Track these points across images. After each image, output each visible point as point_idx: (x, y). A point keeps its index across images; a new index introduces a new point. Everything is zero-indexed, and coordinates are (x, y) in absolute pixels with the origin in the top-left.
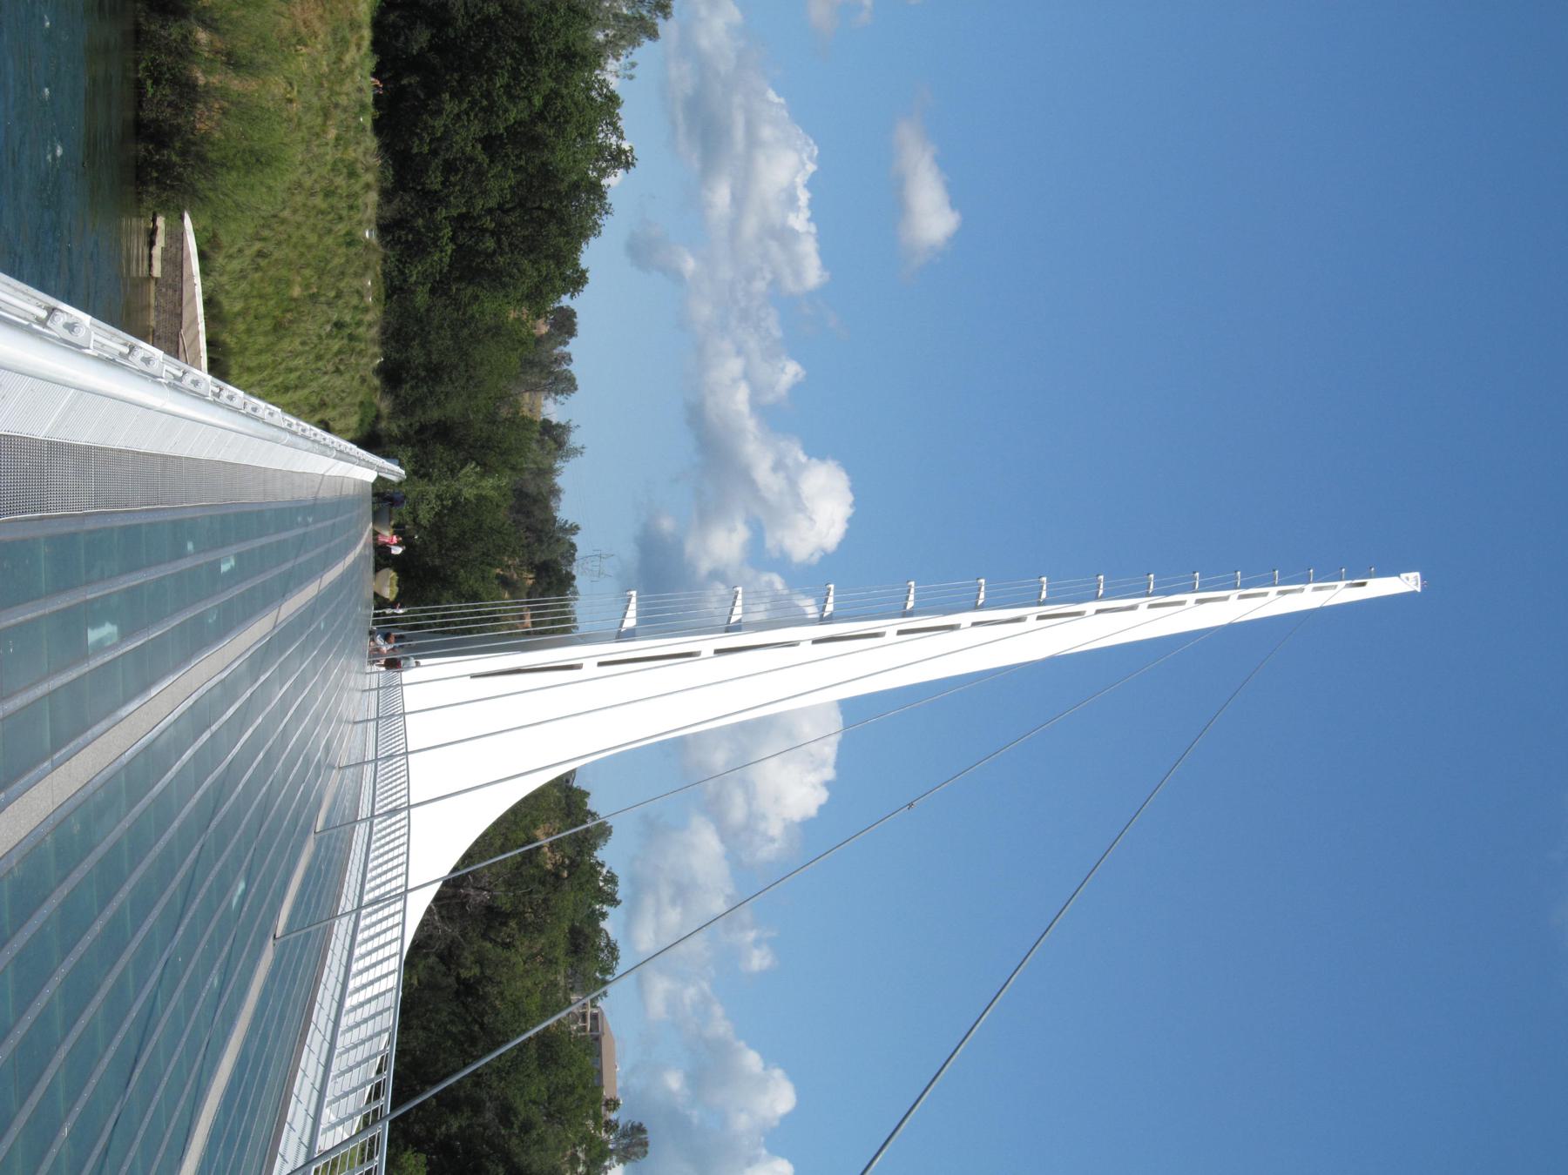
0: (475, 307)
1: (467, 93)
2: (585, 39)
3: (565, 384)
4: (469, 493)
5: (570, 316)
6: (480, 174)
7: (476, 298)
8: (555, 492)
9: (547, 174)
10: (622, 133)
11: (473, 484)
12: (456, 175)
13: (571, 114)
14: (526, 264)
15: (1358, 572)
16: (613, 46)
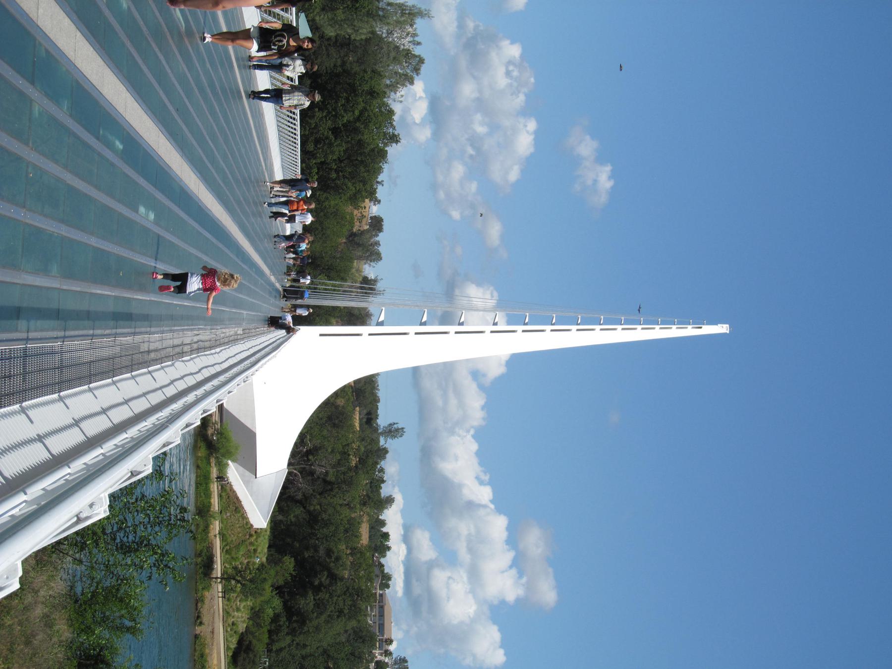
0: (327, 203)
3: (377, 257)
5: (380, 221)
6: (331, 145)
7: (327, 198)
9: (360, 143)
10: (395, 127)
12: (320, 144)
13: (372, 118)
14: (350, 184)
15: (699, 322)
16: (394, 87)
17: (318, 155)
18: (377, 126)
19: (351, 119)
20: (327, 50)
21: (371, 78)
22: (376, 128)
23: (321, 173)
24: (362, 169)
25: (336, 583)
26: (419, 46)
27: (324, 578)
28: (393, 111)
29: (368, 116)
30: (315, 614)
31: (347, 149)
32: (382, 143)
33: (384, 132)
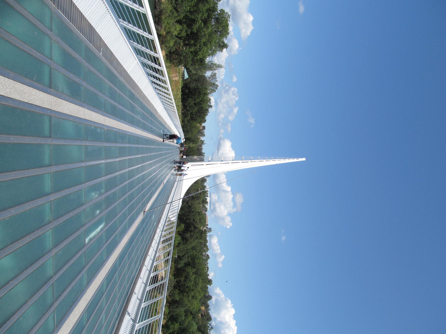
0: (193, 124)
1: (192, 98)
2: (207, 92)
3: (204, 135)
4: (191, 146)
6: (194, 108)
8: (202, 149)
9: (202, 108)
11: (192, 145)
15: (298, 157)
16: (210, 93)
20: (193, 82)
23: (191, 116)
27: (192, 228)
30: (190, 239)
32: (208, 107)
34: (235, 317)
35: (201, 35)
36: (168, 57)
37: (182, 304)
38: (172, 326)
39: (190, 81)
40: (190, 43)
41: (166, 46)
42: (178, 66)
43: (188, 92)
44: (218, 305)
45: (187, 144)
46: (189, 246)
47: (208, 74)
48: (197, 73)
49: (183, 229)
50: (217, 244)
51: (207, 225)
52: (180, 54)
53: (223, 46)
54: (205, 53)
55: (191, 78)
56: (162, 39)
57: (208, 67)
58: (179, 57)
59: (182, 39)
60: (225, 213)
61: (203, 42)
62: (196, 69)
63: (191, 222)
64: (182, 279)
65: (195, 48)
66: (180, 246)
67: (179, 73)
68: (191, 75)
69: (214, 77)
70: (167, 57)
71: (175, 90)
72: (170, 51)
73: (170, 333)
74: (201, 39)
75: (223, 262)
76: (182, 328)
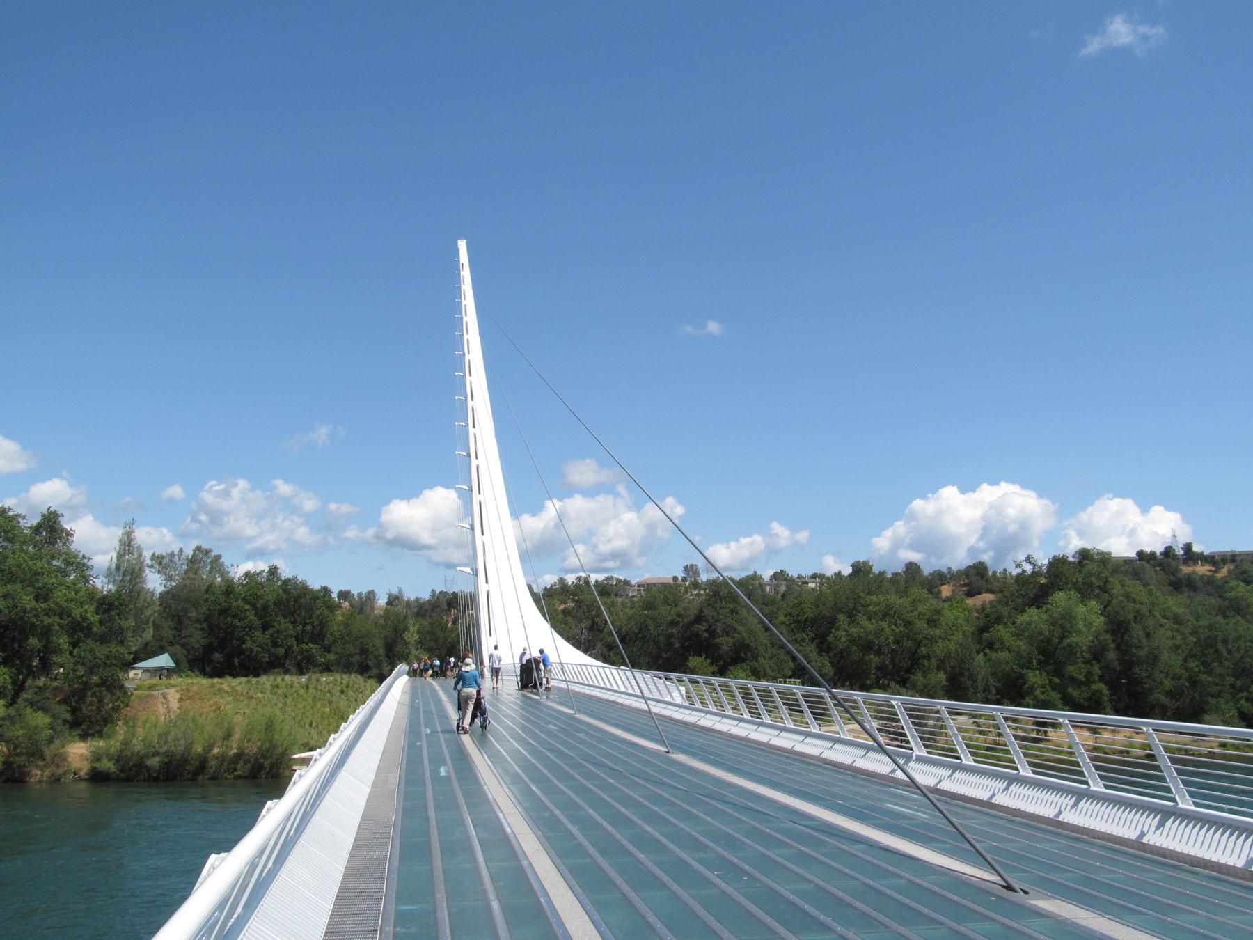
0: (336, 634)
2: (220, 587)
3: (371, 595)
4: (416, 637)
6: (278, 632)
8: (417, 600)
9: (278, 603)
14: (318, 612)
15: (457, 266)
16: (224, 574)
17: (289, 644)
18: (260, 587)
19: (253, 612)
20: (185, 637)
21: (213, 594)
22: (263, 588)
23: (306, 640)
24: (302, 600)
25: (705, 616)
26: (184, 551)
27: (702, 627)
28: (246, 572)
29: (250, 595)
31: (283, 615)
32: (277, 582)
33: (267, 580)
34: (967, 487)
35: (7, 611)
36: (91, 732)
37: (962, 660)
38: (1038, 692)
39: (183, 645)
40: (39, 649)
41: (51, 741)
42: (125, 693)
43: (221, 653)
44: (930, 540)
45: (407, 651)
46: (761, 640)
47: (155, 583)
48: (151, 620)
49: (706, 658)
50: (733, 544)
51: (675, 578)
52: (81, 687)
53: (51, 527)
54: (76, 594)
55: (171, 643)
56: (23, 758)
57: (130, 581)
58: (90, 689)
59: (24, 682)
60: (630, 517)
61: (34, 603)
62: (138, 628)
63: (679, 632)
64: (874, 659)
65: (58, 632)
66: (764, 670)
67: (151, 688)
68: (157, 644)
69: (164, 561)
70: (92, 735)
71: (216, 700)
72: (67, 726)
73: (1061, 699)
74: (25, 611)
75: (794, 528)
76: (1039, 660)
